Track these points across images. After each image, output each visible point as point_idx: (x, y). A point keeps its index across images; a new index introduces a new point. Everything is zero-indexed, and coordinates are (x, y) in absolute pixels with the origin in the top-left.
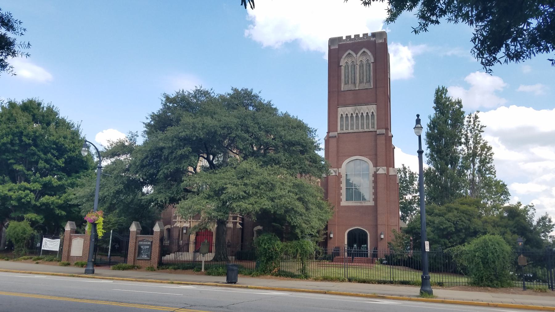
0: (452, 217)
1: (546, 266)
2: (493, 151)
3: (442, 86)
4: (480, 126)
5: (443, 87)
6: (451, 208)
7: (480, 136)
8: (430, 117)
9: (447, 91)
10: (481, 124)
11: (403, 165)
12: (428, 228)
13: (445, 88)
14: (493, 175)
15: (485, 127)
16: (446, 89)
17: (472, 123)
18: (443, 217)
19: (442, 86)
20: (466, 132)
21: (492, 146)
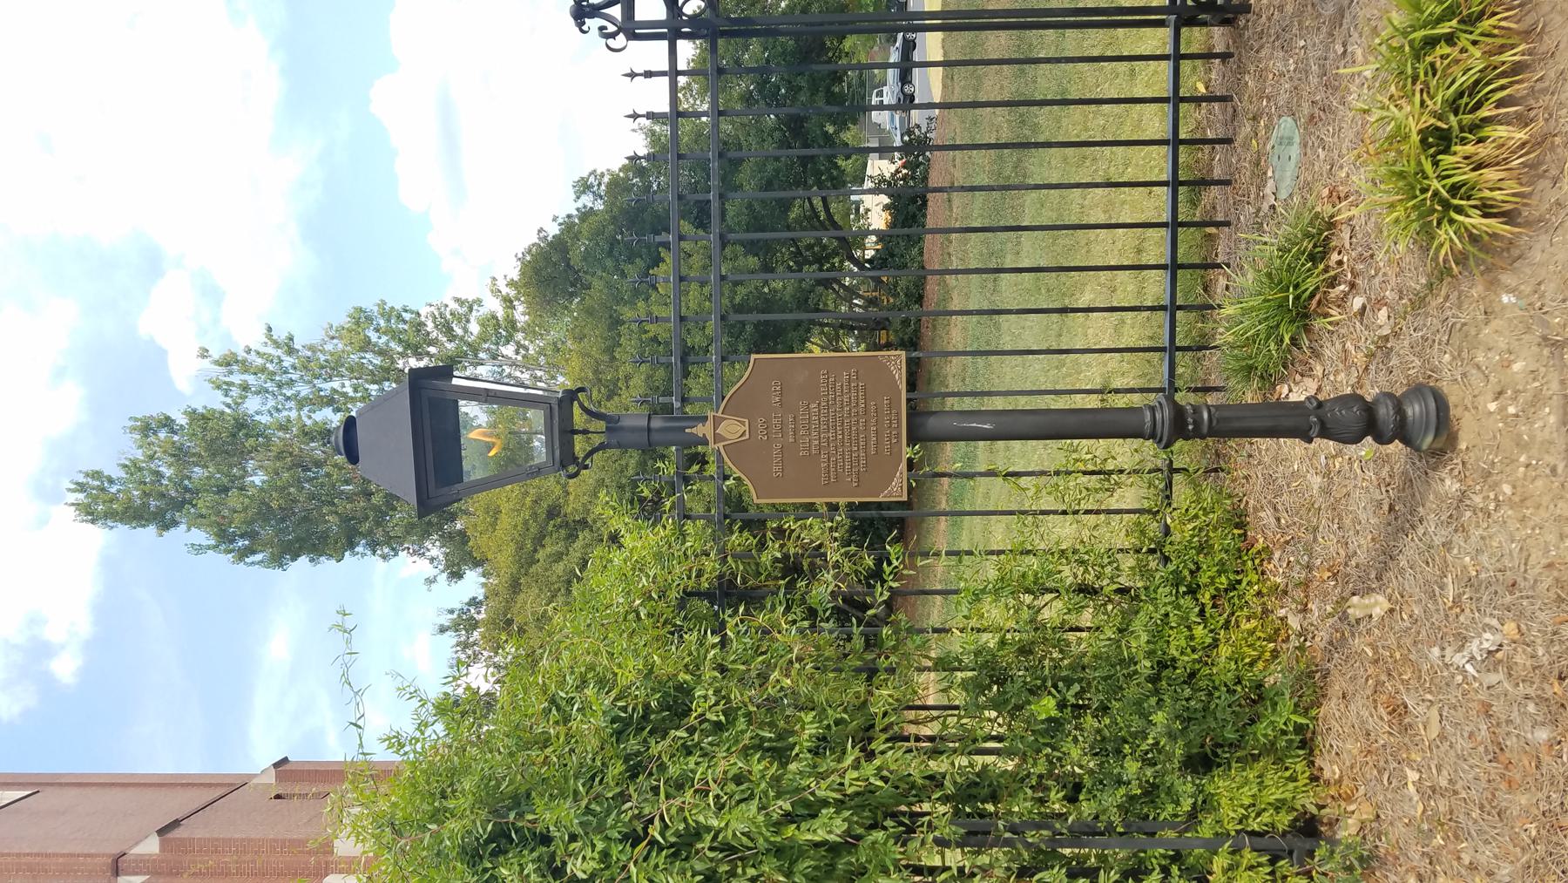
0: (526, 493)
1: (830, 129)
2: (370, 305)
3: (69, 490)
4: (270, 350)
5: (73, 486)
6: (799, 308)
7: (312, 348)
8: (199, 549)
9: (96, 475)
10: (257, 340)
11: (443, 630)
12: (942, 770)
13: (81, 479)
14: (471, 309)
15: (270, 329)
16: (87, 475)
17: (251, 379)
18: (922, 631)
19: (69, 490)
20: (292, 404)
21: (349, 307)
